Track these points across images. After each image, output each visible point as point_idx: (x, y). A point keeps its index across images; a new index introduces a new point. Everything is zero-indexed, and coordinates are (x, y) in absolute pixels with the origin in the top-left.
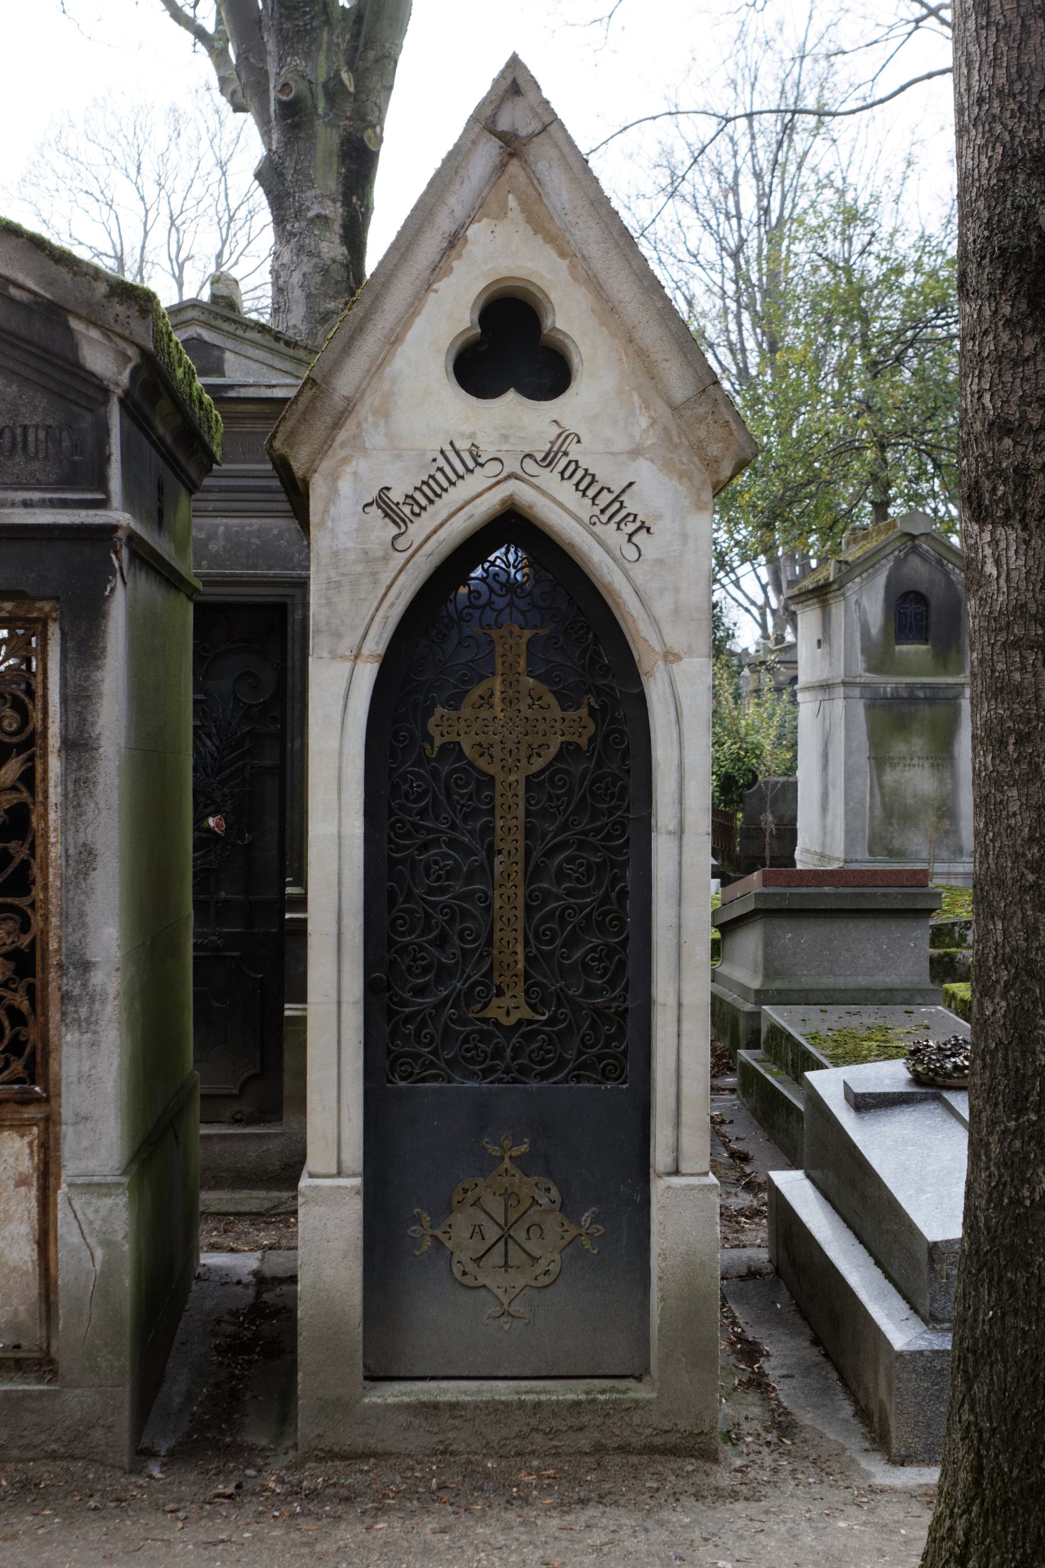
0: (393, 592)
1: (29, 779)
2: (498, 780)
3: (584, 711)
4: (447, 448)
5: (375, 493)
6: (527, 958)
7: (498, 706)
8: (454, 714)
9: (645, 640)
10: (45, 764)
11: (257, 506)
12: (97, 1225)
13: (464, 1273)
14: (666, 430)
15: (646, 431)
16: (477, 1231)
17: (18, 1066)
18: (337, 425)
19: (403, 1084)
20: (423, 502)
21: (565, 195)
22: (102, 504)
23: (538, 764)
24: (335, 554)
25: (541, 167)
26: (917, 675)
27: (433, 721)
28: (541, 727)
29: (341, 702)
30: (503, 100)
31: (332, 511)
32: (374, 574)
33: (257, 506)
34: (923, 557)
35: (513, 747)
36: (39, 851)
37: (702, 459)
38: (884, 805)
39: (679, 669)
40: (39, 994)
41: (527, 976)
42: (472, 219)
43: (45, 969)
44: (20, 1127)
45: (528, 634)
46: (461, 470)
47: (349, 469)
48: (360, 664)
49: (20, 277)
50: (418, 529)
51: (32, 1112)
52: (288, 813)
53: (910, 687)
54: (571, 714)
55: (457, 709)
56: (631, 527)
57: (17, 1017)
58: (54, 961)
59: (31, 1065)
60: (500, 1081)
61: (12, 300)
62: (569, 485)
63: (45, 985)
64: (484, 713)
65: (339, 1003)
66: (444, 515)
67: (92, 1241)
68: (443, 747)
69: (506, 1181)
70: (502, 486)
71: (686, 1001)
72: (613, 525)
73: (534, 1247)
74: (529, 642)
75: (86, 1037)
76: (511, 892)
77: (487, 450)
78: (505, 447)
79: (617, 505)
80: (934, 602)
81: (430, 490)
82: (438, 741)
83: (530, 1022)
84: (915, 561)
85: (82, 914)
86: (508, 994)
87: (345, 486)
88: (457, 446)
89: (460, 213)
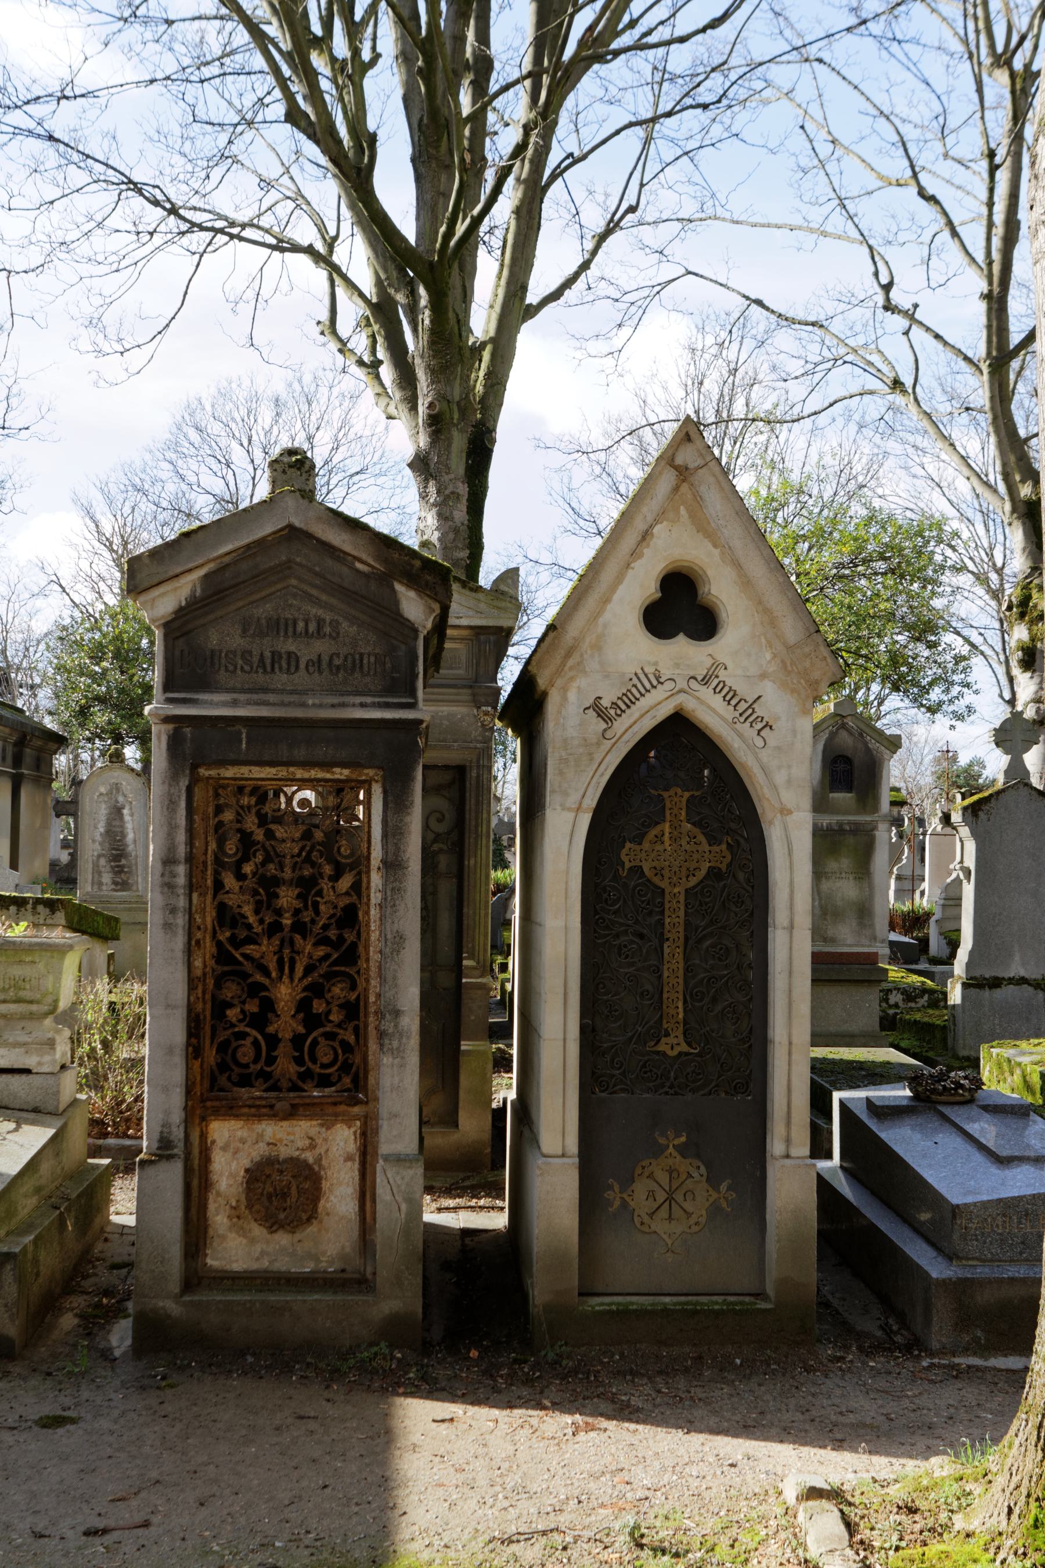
0: (603, 766)
1: (358, 888)
2: (667, 891)
3: (724, 847)
4: (639, 672)
5: (592, 701)
6: (685, 1011)
7: (667, 842)
8: (638, 848)
10: (369, 877)
11: (446, 697)
12: (403, 1188)
13: (642, 1223)
14: (783, 661)
15: (770, 662)
16: (651, 1195)
17: (347, 1081)
18: (568, 655)
20: (623, 707)
21: (719, 507)
22: (412, 706)
23: (693, 881)
24: (565, 741)
25: (703, 489)
26: (844, 814)
27: (624, 851)
28: (696, 856)
30: (680, 444)
31: (564, 712)
32: (590, 754)
33: (446, 697)
34: (849, 731)
36: (363, 936)
37: (806, 681)
38: (821, 907)
39: (792, 819)
40: (362, 1031)
41: (685, 1023)
42: (656, 521)
43: (366, 1015)
44: (348, 1122)
45: (687, 794)
46: (648, 686)
47: (575, 684)
48: (581, 814)
49: (364, 557)
50: (620, 725)
51: (356, 1110)
52: (465, 910)
53: (840, 824)
54: (715, 848)
55: (640, 844)
56: (759, 726)
57: (346, 1047)
58: (372, 1009)
59: (356, 1081)
60: (667, 1093)
61: (357, 571)
62: (719, 698)
63: (366, 1026)
64: (659, 847)
65: (565, 1040)
66: (637, 715)
67: (399, 1199)
68: (631, 869)
69: (670, 1161)
70: (676, 697)
71: (795, 1041)
72: (748, 724)
73: (688, 1206)
74: (688, 801)
75: (396, 1061)
76: (675, 967)
77: (666, 674)
78: (677, 672)
79: (750, 711)
80: (856, 762)
81: (628, 700)
82: (627, 865)
83: (687, 1054)
84: (843, 734)
85: (395, 978)
87: (572, 696)
88: (646, 670)
89: (650, 518)
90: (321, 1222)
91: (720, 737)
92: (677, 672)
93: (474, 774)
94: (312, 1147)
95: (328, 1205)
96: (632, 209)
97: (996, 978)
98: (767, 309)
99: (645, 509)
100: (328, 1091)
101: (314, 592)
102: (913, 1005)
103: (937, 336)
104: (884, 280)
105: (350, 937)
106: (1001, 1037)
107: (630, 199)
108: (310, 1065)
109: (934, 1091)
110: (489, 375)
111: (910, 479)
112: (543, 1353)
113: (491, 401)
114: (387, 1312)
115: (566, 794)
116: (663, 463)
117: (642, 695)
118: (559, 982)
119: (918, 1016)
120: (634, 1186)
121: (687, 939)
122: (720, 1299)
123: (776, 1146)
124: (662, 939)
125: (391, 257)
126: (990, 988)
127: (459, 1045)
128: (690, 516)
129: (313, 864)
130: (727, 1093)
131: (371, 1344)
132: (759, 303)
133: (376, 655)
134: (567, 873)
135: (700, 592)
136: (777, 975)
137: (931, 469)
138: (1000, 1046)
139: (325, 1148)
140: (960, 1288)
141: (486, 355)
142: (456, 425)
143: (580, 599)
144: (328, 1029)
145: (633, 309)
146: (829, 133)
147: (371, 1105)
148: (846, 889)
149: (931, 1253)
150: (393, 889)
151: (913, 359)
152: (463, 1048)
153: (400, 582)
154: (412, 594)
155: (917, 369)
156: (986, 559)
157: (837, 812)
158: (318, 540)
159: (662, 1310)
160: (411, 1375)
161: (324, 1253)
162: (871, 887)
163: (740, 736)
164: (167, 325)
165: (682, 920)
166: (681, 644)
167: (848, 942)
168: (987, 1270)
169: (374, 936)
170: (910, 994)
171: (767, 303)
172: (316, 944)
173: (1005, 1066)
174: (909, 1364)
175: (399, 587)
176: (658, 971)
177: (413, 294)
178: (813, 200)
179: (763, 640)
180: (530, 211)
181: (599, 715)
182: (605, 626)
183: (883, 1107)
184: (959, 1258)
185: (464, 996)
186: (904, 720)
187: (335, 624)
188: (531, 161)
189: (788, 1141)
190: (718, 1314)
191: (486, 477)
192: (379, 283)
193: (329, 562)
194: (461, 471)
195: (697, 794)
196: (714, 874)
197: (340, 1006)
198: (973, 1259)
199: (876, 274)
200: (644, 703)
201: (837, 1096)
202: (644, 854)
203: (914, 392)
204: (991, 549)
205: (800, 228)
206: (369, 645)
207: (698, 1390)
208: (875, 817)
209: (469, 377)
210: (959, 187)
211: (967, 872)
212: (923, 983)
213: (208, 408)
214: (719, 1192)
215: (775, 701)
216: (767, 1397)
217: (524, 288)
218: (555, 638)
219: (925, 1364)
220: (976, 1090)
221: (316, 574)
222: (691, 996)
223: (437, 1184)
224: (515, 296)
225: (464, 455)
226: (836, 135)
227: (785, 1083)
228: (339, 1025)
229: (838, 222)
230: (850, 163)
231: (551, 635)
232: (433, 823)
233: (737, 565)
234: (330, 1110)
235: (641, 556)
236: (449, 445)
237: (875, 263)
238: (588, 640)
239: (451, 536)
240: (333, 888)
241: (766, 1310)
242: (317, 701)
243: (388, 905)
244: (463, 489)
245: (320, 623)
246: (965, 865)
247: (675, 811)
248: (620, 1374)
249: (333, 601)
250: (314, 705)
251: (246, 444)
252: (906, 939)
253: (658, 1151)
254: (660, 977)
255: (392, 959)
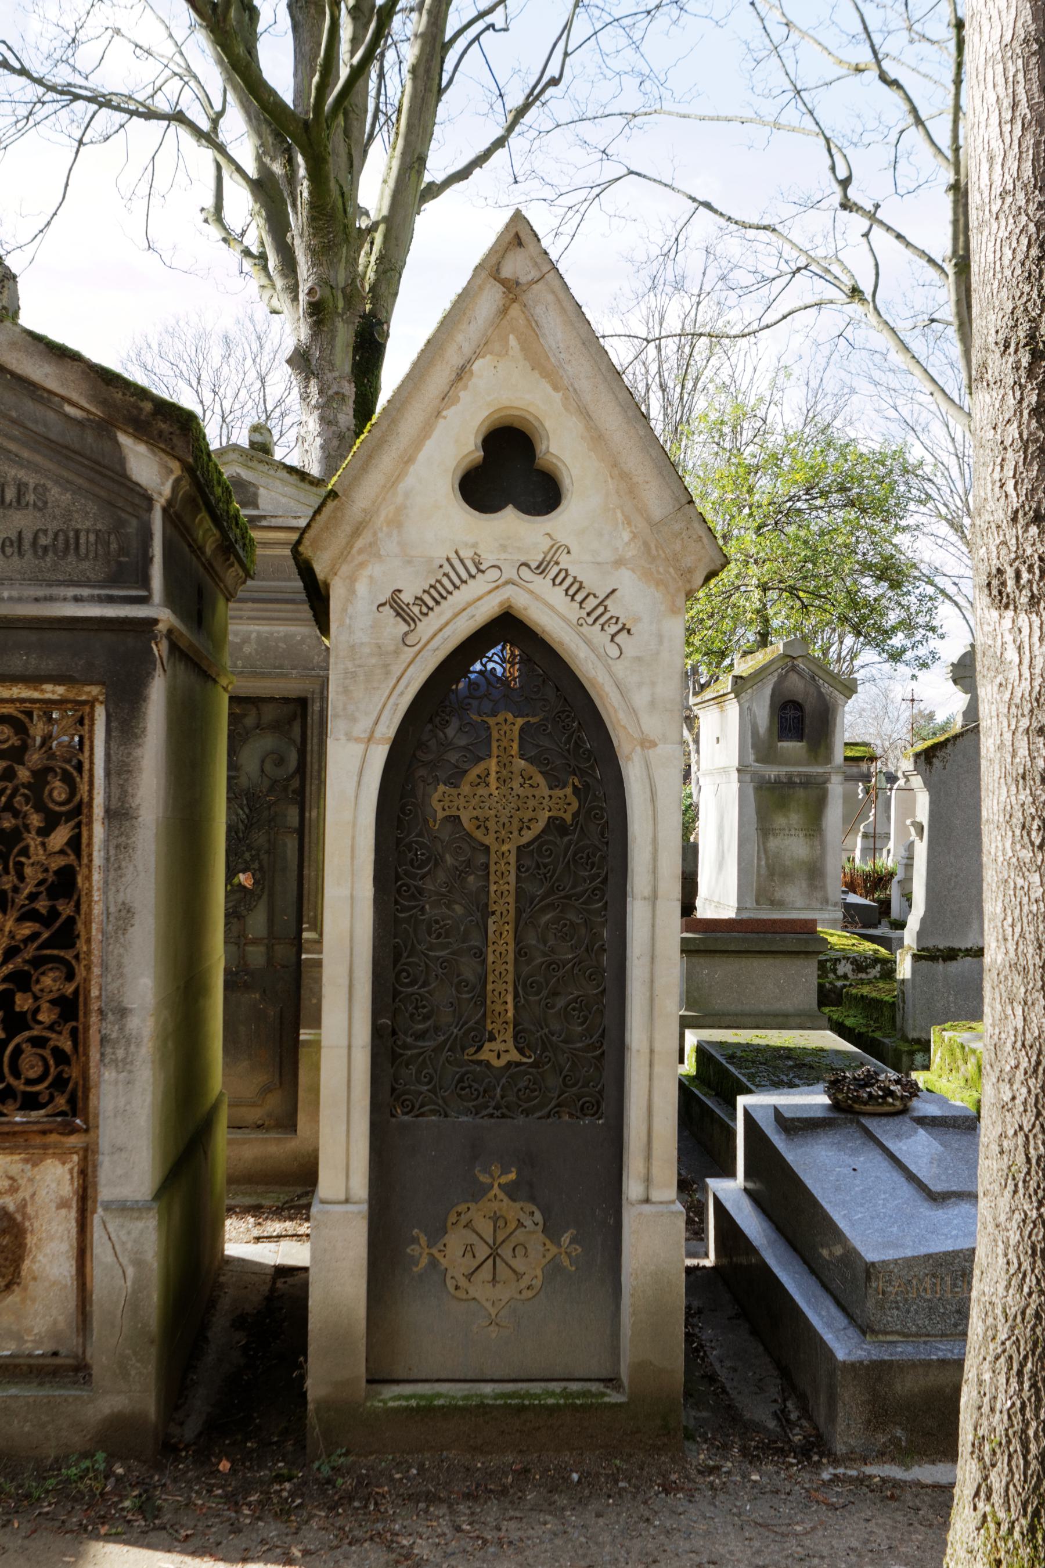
1: (75, 844)
2: (493, 850)
3: (569, 790)
6: (516, 1007)
7: (493, 784)
8: (454, 791)
9: (624, 728)
12: (129, 1246)
13: (457, 1288)
14: (646, 544)
15: (628, 544)
16: (469, 1250)
17: (61, 1101)
18: (357, 531)
19: (406, 1118)
20: (431, 603)
22: (144, 600)
23: (528, 836)
24: (352, 647)
25: (539, 310)
26: (795, 764)
27: (436, 796)
28: (531, 803)
29: (356, 778)
31: (350, 610)
32: (386, 666)
33: (276, 614)
35: (506, 821)
36: (84, 908)
37: (676, 569)
38: (768, 866)
40: (81, 1036)
42: (477, 355)
43: (87, 1014)
44: (62, 1156)
45: (520, 721)
47: (366, 572)
48: (373, 747)
49: (74, 396)
50: (426, 627)
51: (73, 1140)
52: (306, 872)
53: (790, 776)
54: (558, 793)
56: (614, 629)
57: (61, 1057)
59: (72, 1101)
60: (491, 1116)
61: (67, 416)
62: (560, 591)
63: (87, 1028)
64: (481, 791)
65: (349, 1047)
66: (448, 615)
67: (124, 1261)
69: (495, 1205)
70: (501, 591)
71: (658, 1047)
72: (598, 626)
73: (518, 1264)
74: (522, 729)
76: (502, 949)
77: (488, 559)
78: (503, 556)
79: (601, 609)
80: (808, 709)
81: (436, 594)
82: (440, 815)
83: (518, 1064)
84: (794, 677)
85: (120, 965)
86: (499, 1040)
87: (362, 588)
88: (462, 554)
89: (467, 350)
90: (25, 1289)
91: (561, 643)
92: (503, 556)
93: (317, 707)
94: (13, 1189)
95: (35, 1267)
96: (554, 82)
97: (952, 949)
98: (715, 211)
99: (460, 338)
100: (35, 1115)
101: (12, 447)
102: (863, 976)
103: (899, 236)
104: (842, 174)
105: (66, 909)
106: (956, 1017)
107: (553, 71)
108: (11, 1080)
109: (857, 1099)
110: (381, 259)
111: (882, 421)
112: (316, 1465)
113: (383, 289)
114: (107, 1411)
115: (353, 719)
116: (484, 274)
117: (456, 587)
118: (343, 970)
119: (865, 990)
120: (446, 1239)
121: (519, 911)
122: (556, 1387)
123: (633, 1189)
124: (486, 912)
125: (265, 119)
126: (944, 960)
127: (298, 1035)
128: (523, 349)
129: (16, 814)
130: (571, 1115)
131: (88, 1455)
132: (708, 205)
133: (97, 533)
134: (354, 825)
135: (538, 452)
136: (636, 962)
137: (905, 412)
138: (953, 1028)
139: (30, 1191)
140: (875, 1373)
141: (379, 237)
142: (342, 316)
143: (370, 457)
144: (35, 1033)
145: (570, 213)
146: (783, 14)
147: (92, 1134)
148: (795, 847)
149: (841, 1321)
150: (117, 847)
151: (873, 263)
152: (302, 1037)
153: (125, 432)
154: (142, 448)
155: (877, 274)
156: (960, 505)
157: (787, 763)
158: (12, 374)
159: (478, 1406)
160: (127, 1503)
161: (29, 1331)
162: (823, 844)
163: (588, 642)
164: (49, 223)
165: (512, 887)
166: (509, 520)
167: (798, 905)
168: (910, 1349)
169: (97, 909)
170: (860, 965)
171: (715, 205)
172: (20, 919)
173: (958, 1051)
174: (805, 1476)
175: (124, 439)
176: (480, 955)
177: (291, 161)
178: (766, 91)
179: (619, 515)
180: (428, 71)
181: (398, 614)
182: (407, 495)
183: (793, 1119)
184: (873, 1332)
185: (304, 975)
186: (878, 676)
187: (41, 490)
188: (429, 12)
189: (648, 1180)
190: (552, 1410)
191: (377, 377)
192: (259, 158)
193: (30, 406)
194: (347, 368)
195: (532, 720)
196: (555, 826)
197: (52, 1002)
198: (892, 1333)
199: (833, 169)
200: (459, 598)
201: (742, 1101)
202: (462, 802)
203: (874, 301)
204: (967, 494)
205: (751, 121)
206: (88, 519)
207: (513, 1525)
208: (827, 768)
209: (356, 260)
210: (925, 76)
211: (920, 829)
212: (876, 951)
213: (155, 346)
214: (559, 1245)
215: (635, 596)
216: (605, 1537)
217: (422, 160)
218: (336, 509)
219: (826, 1476)
220: (910, 1098)
221: (13, 421)
222: (523, 985)
223: (266, 1203)
224: (411, 168)
225: (351, 349)
226: (791, 17)
227: (644, 1103)
228: (51, 1028)
229: (793, 115)
230: (807, 48)
231: (331, 505)
232: (268, 767)
233: (585, 414)
234: (38, 1140)
235: (456, 400)
236: (333, 338)
237: (831, 156)
238: (383, 514)
239: (335, 443)
240: (43, 844)
241: (616, 1405)
242: (15, 594)
243: (114, 867)
244: (349, 390)
245: (21, 488)
246: (918, 820)
247: (504, 743)
248: (413, 1498)
249: (38, 459)
250: (11, 599)
251: (195, 384)
252: (866, 902)
253: (478, 1193)
254: (484, 962)
255: (117, 940)
